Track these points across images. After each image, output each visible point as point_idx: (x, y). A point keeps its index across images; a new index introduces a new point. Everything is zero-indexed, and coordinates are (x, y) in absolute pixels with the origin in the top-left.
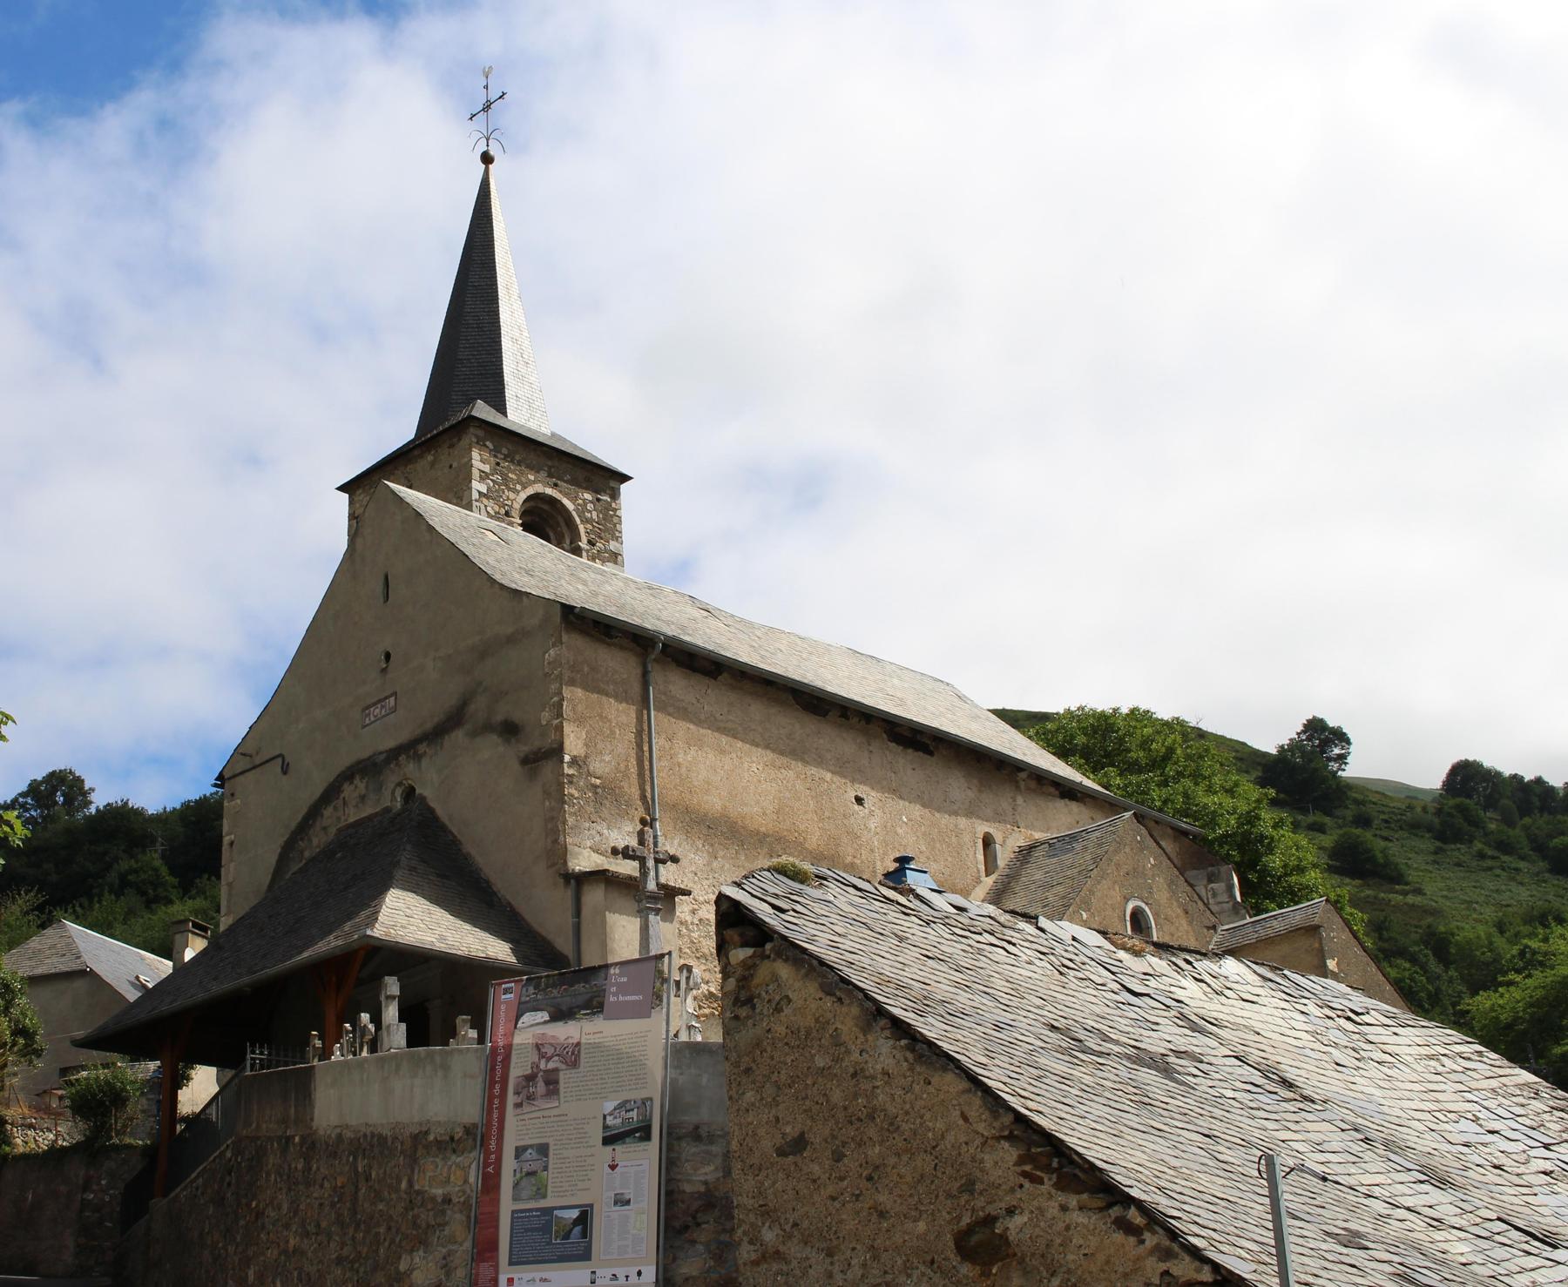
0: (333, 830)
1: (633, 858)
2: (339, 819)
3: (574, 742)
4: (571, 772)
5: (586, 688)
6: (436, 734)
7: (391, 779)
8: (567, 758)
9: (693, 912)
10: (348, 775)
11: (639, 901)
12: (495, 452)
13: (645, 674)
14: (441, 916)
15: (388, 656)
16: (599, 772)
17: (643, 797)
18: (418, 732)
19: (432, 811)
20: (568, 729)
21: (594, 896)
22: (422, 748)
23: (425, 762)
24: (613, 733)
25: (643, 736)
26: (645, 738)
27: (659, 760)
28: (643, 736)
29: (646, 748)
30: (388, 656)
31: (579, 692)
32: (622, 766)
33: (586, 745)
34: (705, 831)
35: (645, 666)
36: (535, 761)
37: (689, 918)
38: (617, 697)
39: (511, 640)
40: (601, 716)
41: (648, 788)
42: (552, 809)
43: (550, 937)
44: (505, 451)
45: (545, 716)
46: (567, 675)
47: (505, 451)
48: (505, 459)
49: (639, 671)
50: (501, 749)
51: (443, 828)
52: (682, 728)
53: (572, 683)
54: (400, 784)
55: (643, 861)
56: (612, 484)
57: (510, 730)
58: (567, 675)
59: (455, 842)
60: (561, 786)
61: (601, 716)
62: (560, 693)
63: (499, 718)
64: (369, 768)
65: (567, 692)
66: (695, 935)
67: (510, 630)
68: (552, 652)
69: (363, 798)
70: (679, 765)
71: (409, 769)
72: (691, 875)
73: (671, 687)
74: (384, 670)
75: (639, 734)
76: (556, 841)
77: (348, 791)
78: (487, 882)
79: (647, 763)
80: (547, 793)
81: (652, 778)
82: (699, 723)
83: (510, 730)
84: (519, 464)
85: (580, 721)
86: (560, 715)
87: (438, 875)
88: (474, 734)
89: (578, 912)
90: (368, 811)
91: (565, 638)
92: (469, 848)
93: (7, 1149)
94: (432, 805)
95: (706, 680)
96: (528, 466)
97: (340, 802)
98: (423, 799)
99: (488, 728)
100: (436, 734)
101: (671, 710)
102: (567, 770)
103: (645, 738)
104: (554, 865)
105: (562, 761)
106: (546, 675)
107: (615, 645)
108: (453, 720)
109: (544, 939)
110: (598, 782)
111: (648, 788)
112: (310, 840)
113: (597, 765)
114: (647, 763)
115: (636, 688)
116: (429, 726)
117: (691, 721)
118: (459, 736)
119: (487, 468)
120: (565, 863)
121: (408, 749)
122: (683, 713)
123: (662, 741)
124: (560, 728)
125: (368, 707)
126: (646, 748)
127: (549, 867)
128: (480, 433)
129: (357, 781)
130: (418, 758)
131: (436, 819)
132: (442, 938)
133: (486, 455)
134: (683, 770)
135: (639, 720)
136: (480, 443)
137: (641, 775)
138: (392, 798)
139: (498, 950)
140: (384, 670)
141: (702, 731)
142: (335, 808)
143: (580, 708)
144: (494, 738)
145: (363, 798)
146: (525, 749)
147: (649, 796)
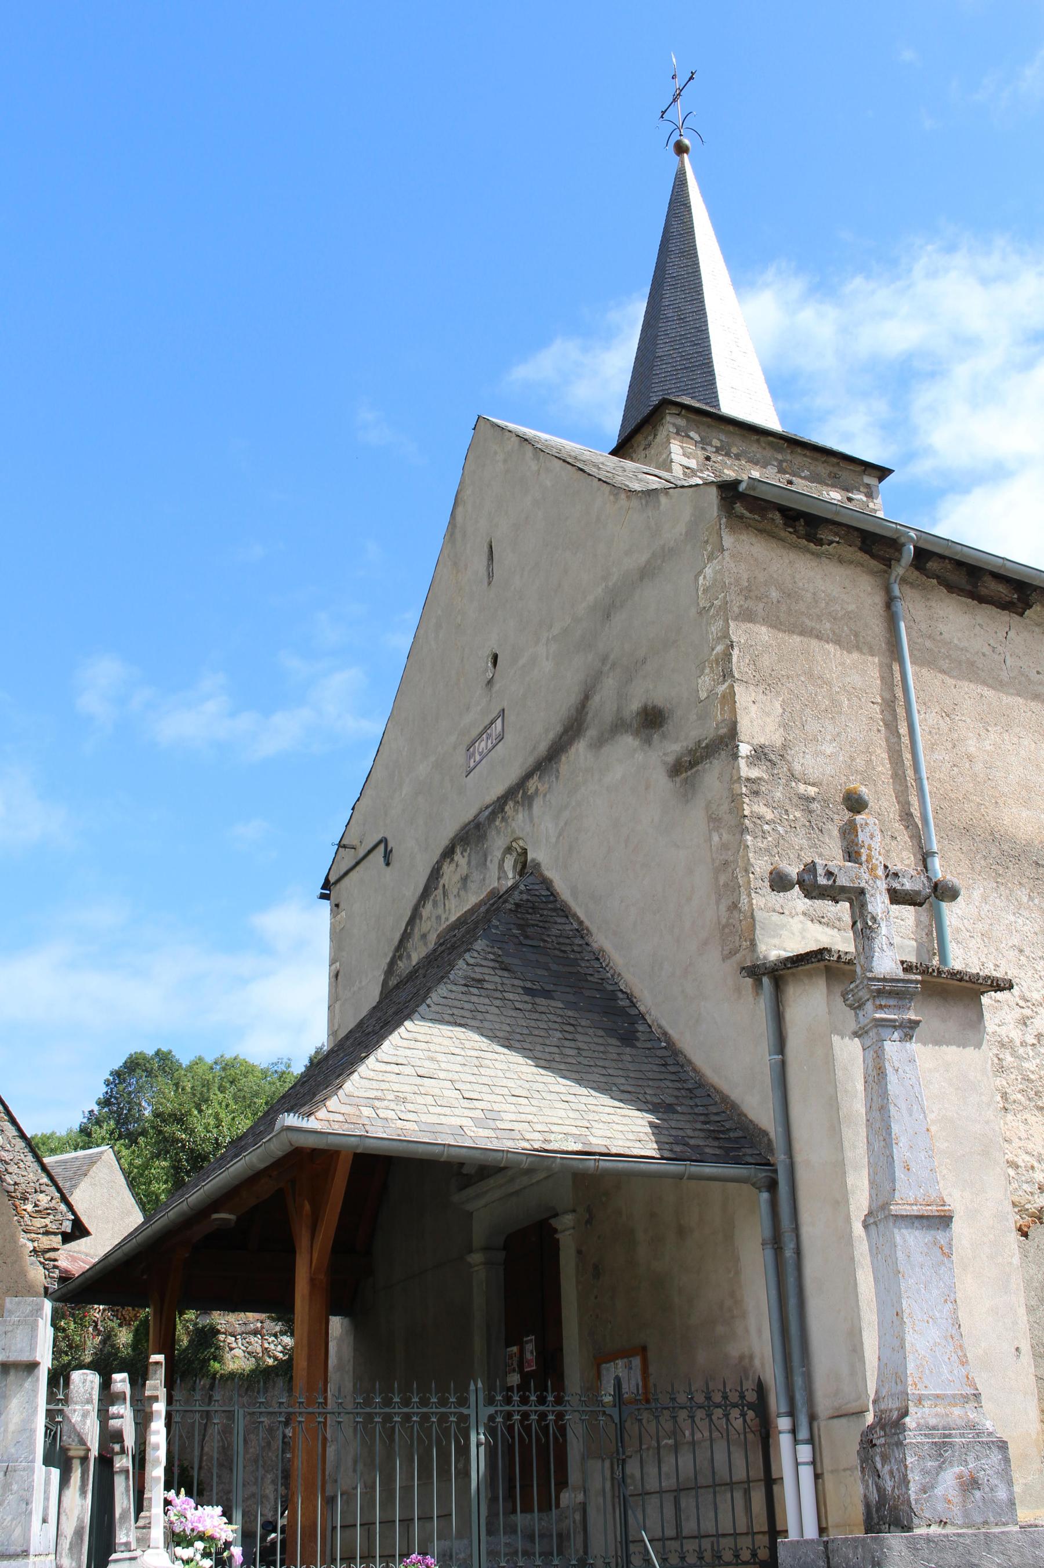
0: (432, 938)
1: (833, 893)
2: (438, 918)
3: (758, 721)
4: (754, 773)
5: (775, 624)
6: (548, 761)
7: (497, 843)
8: (744, 749)
9: (1024, 1022)
10: (448, 853)
11: (857, 1007)
12: (704, 443)
13: (889, 603)
14: (512, 1069)
15: (495, 658)
16: (814, 774)
17: (906, 816)
18: (531, 761)
19: (547, 883)
20: (743, 696)
21: (809, 1004)
22: (532, 784)
23: (537, 804)
24: (835, 703)
25: (895, 709)
26: (901, 712)
27: (932, 747)
28: (895, 709)
29: (903, 730)
30: (495, 658)
31: (763, 633)
32: (860, 763)
33: (785, 726)
34: (1031, 872)
35: (888, 589)
36: (692, 765)
37: (1016, 1035)
38: (838, 642)
39: (646, 573)
40: (810, 674)
41: (914, 800)
42: (725, 847)
43: (735, 1095)
44: (716, 442)
45: (705, 682)
46: (736, 603)
47: (716, 442)
48: (718, 450)
49: (879, 599)
50: (639, 757)
51: (564, 912)
52: (969, 694)
53: (748, 616)
54: (509, 850)
55: (857, 897)
56: (867, 480)
57: (652, 720)
58: (736, 603)
59: (582, 931)
60: (736, 799)
61: (810, 674)
62: (726, 635)
63: (635, 706)
64: (471, 836)
65: (738, 632)
66: (1030, 1065)
67: (643, 558)
68: (708, 571)
69: (465, 880)
70: (970, 758)
71: (518, 820)
72: (1013, 954)
73: (941, 627)
74: (490, 682)
75: (889, 705)
76: (734, 906)
77: (450, 875)
78: (629, 997)
79: (907, 756)
80: (714, 821)
81: (919, 780)
82: (999, 685)
83: (652, 720)
84: (738, 457)
85: (768, 683)
86: (727, 674)
87: (528, 991)
88: (599, 743)
89: (780, 1043)
90: (472, 899)
91: (728, 540)
92: (601, 940)
93: (217, 1365)
94: (549, 874)
95: (1005, 616)
96: (750, 461)
97: (440, 891)
98: (537, 865)
99: (619, 726)
100: (548, 761)
101: (945, 665)
102: (746, 770)
103: (901, 712)
104: (733, 953)
105: (735, 756)
106: (702, 612)
107: (829, 557)
108: (572, 729)
109: (725, 1099)
110: (812, 791)
111: (914, 800)
112: (409, 957)
113: (809, 760)
114: (907, 756)
115: (875, 627)
116: (543, 748)
117: (984, 683)
118: (580, 751)
119: (693, 464)
120: (753, 944)
121: (517, 793)
122: (969, 669)
123: (932, 718)
124: (729, 699)
125: (473, 743)
126: (903, 730)
127: (725, 958)
128: (681, 422)
129: (458, 857)
130: (528, 801)
131: (553, 895)
132: (490, 1117)
133: (691, 447)
134: (979, 767)
135: (887, 681)
136: (682, 433)
137: (898, 776)
138: (499, 875)
139: (618, 1129)
140: (490, 682)
141: (1008, 700)
142: (435, 904)
143: (766, 661)
144: (628, 741)
145: (465, 880)
146: (674, 748)
147: (916, 813)
